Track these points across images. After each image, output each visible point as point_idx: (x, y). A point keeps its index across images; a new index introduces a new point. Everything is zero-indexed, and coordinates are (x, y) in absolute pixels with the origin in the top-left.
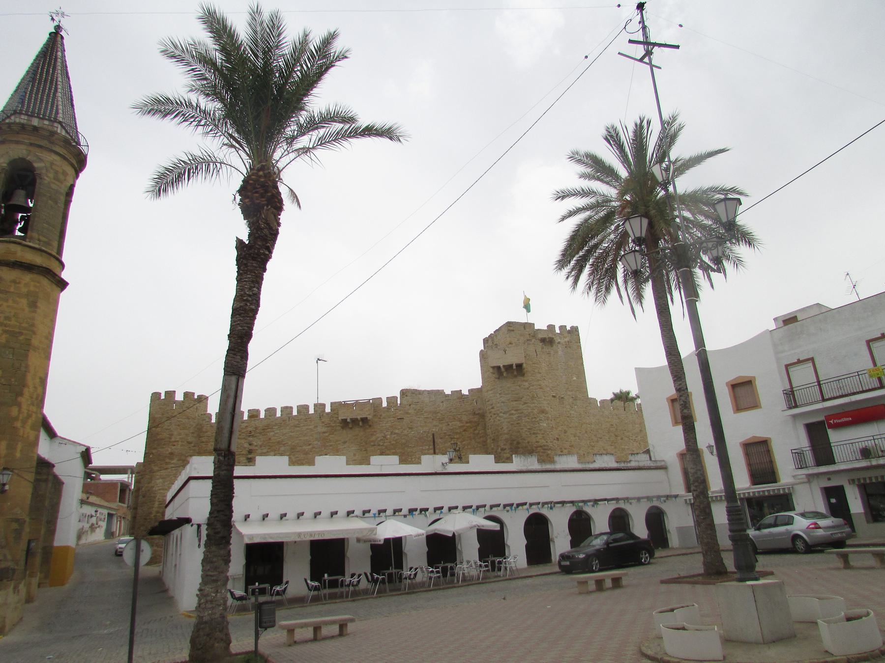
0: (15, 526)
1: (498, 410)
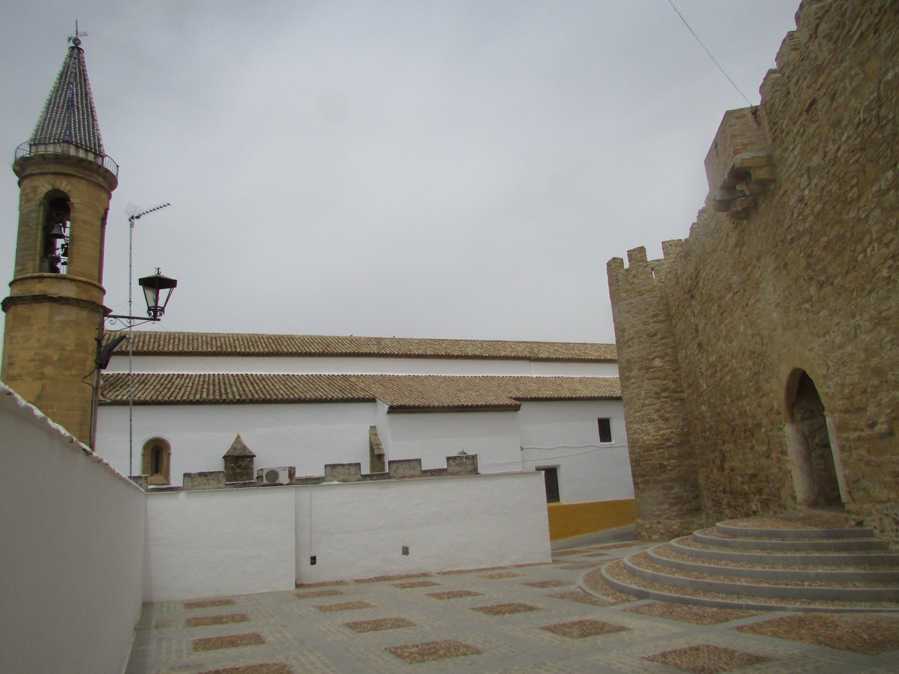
0: (642, 486)
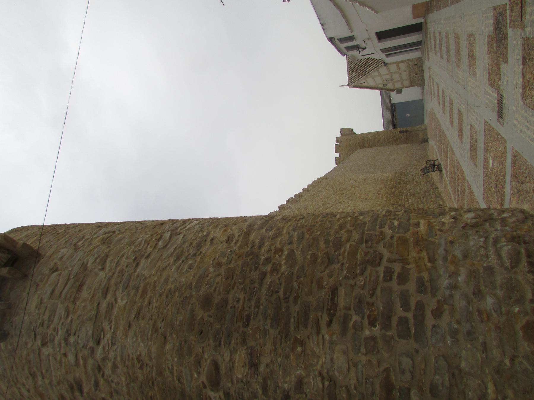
1: (85, 360)
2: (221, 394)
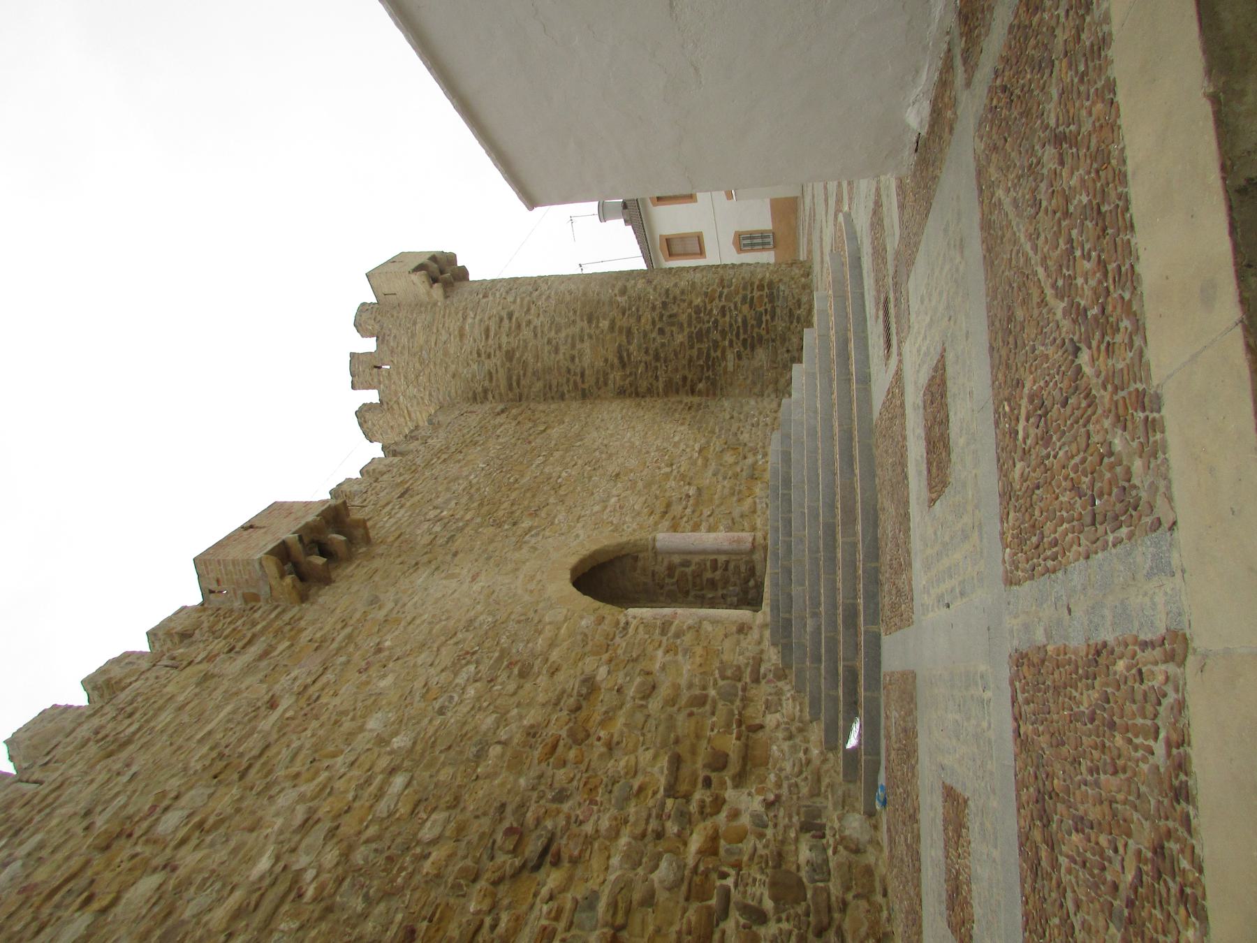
2: (626, 298)
